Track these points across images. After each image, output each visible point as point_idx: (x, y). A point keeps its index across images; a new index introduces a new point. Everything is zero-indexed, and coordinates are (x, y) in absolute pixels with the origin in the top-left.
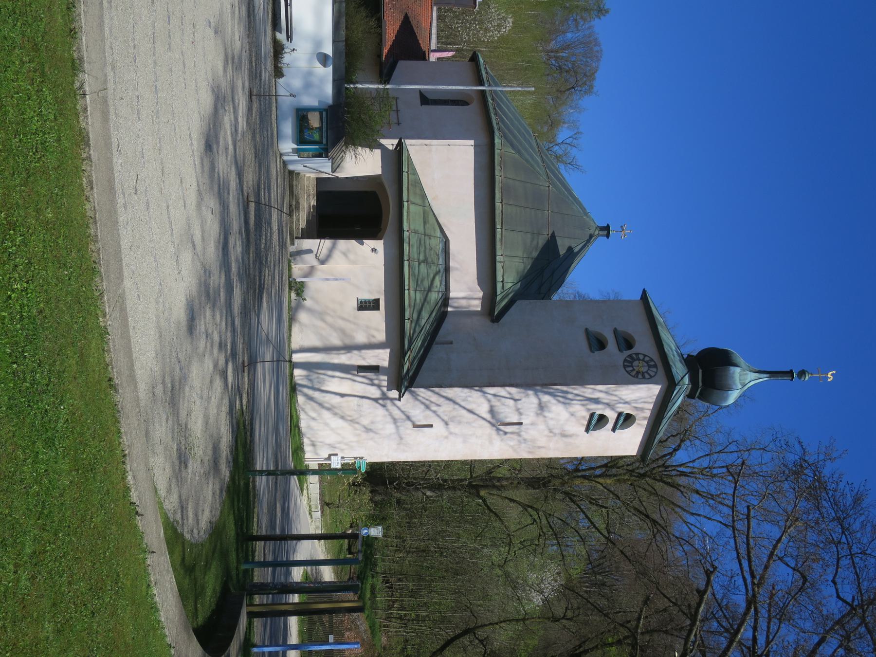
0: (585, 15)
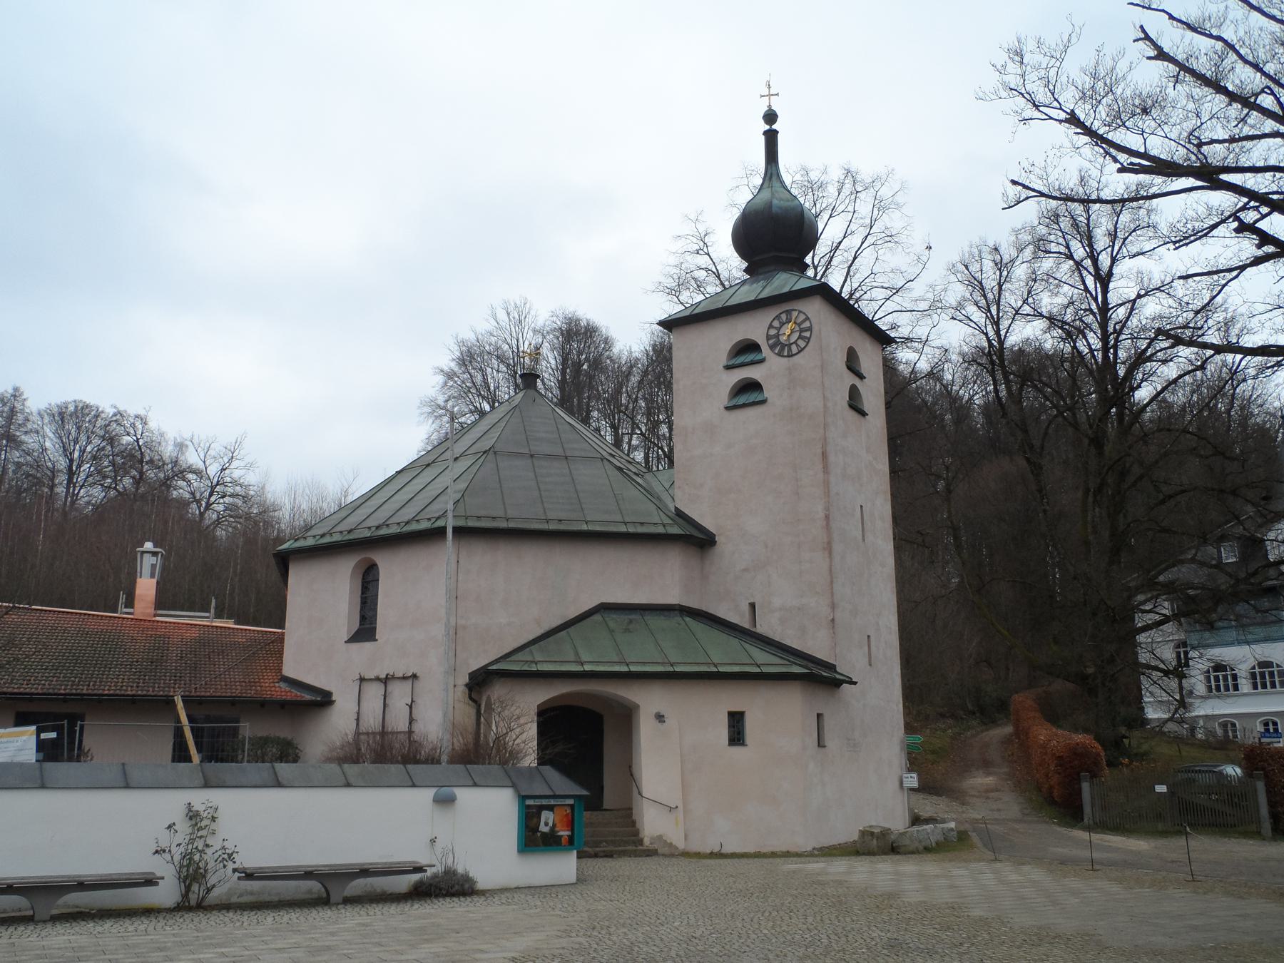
0: (20, 418)
